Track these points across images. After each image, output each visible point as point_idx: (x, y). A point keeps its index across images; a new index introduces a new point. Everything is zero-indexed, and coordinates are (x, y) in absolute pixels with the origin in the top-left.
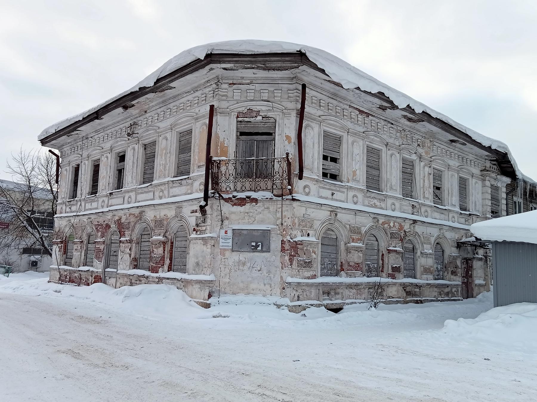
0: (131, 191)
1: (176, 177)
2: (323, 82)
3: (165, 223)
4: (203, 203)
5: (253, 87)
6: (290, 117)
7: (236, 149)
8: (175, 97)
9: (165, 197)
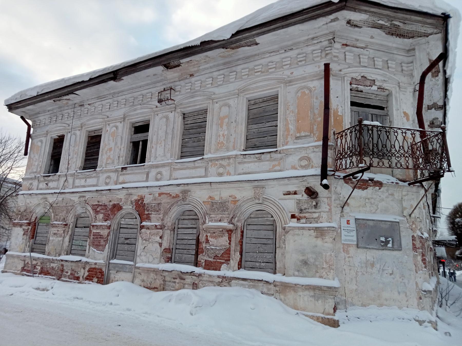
0: (163, 166)
3: (231, 206)
5: (367, 53)
6: (406, 92)
9: (229, 174)
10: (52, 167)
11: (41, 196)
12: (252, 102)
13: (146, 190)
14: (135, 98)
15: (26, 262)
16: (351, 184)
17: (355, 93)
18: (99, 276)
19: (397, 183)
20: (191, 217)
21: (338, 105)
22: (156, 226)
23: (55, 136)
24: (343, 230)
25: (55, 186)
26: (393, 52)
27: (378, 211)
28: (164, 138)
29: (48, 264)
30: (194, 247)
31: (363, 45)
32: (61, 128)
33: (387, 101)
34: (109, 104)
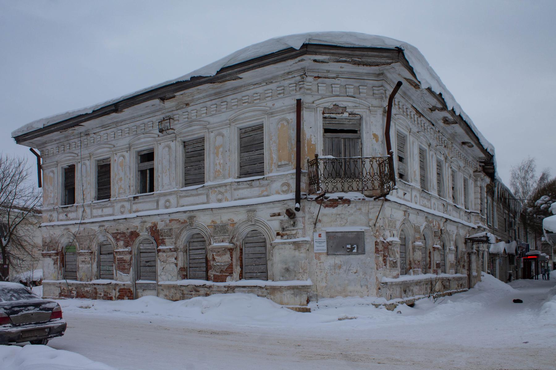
0: (170, 194)
1: (240, 178)
3: (230, 228)
4: (293, 205)
6: (376, 114)
8: (236, 88)
9: (227, 200)
10: (67, 197)
11: (64, 227)
12: (243, 131)
13: (158, 218)
14: (138, 127)
15: (62, 288)
18: (127, 294)
19: (363, 199)
20: (199, 240)
21: (311, 136)
22: (170, 249)
23: (65, 166)
25: (75, 217)
26: (363, 78)
27: (348, 223)
28: (168, 167)
29: (82, 289)
30: (204, 265)
31: (334, 75)
32: (71, 158)
33: (360, 124)
34: (113, 133)
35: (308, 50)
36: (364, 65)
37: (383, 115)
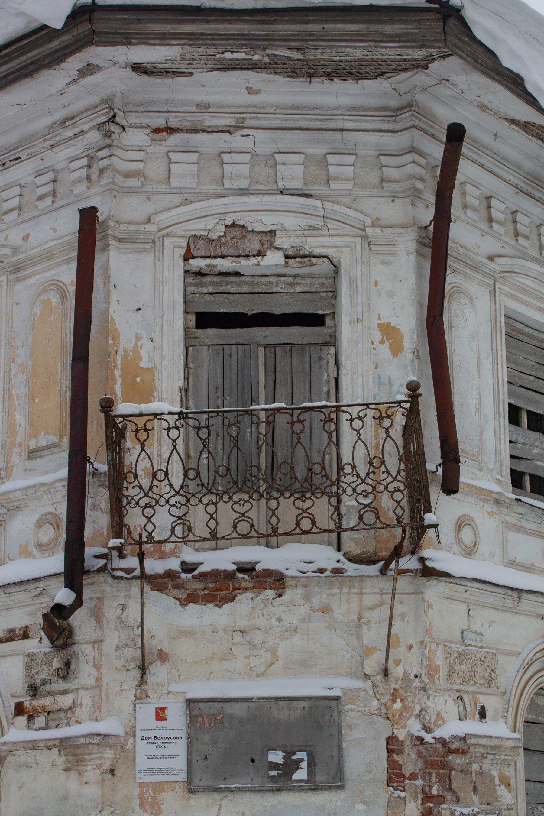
2: (504, 128)
4: (64, 596)
5: (247, 143)
6: (393, 253)
7: (186, 378)
16: (176, 591)
17: (214, 284)
19: (337, 571)
21: (138, 338)
24: (143, 738)
26: (340, 125)
27: (278, 665)
35: (98, 27)
36: (330, 76)
37: (419, 254)
